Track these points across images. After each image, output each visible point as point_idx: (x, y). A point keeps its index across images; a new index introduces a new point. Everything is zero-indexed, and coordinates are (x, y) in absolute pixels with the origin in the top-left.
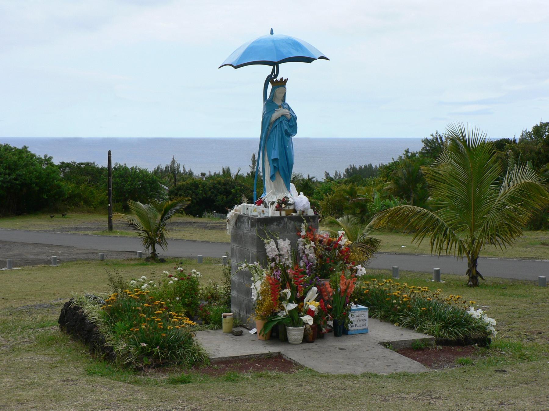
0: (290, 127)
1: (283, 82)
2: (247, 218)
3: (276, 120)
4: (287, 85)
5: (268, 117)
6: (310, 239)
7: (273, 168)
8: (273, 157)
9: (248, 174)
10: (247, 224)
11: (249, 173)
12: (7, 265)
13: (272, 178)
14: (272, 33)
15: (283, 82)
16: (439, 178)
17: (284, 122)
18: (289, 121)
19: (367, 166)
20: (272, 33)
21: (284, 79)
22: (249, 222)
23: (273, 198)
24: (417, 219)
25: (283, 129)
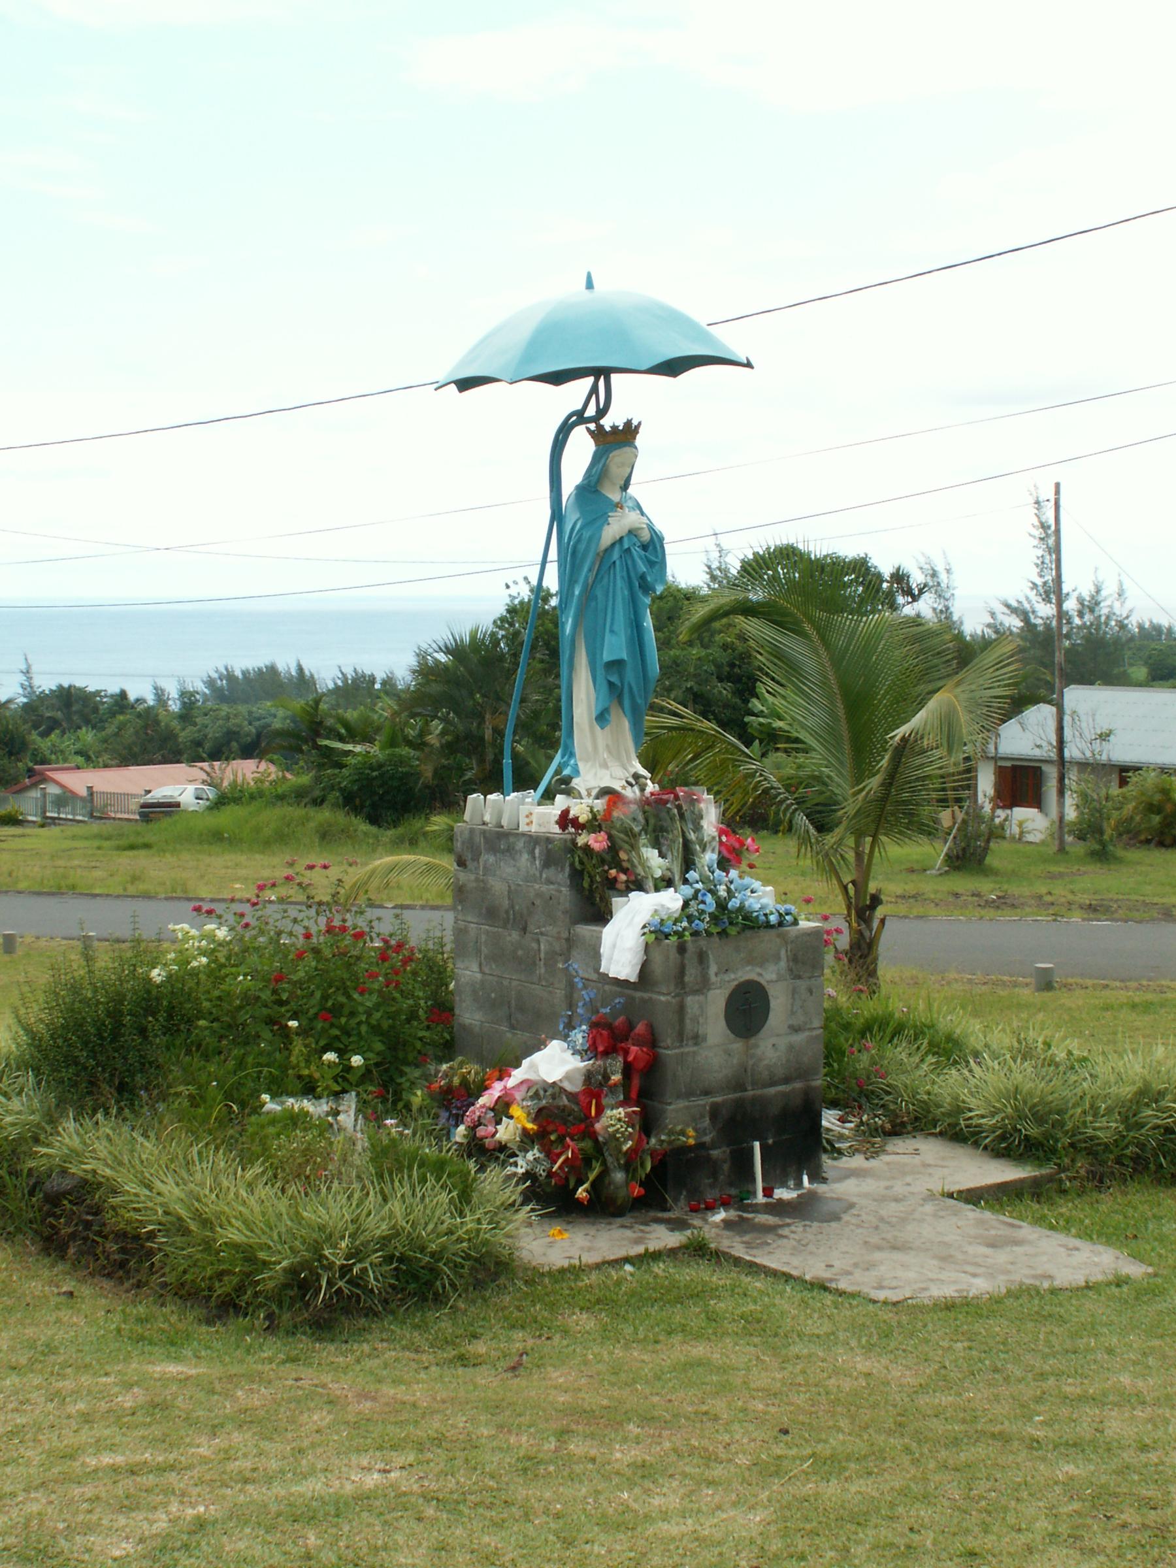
0: (651, 564)
1: (627, 434)
2: (523, 840)
3: (613, 545)
4: (639, 441)
5: (590, 539)
6: (68, 1516)
7: (604, 688)
8: (607, 657)
9: (160, 694)
10: (525, 856)
11: (172, 691)
12: (1122, 669)
13: (602, 718)
14: (590, 285)
15: (627, 434)
16: (590, 570)
17: (637, 552)
18: (645, 547)
19: (372, 680)
20: (590, 285)
21: (635, 423)
22: (537, 851)
23: (601, 779)
24: (934, 680)
25: (632, 574)
